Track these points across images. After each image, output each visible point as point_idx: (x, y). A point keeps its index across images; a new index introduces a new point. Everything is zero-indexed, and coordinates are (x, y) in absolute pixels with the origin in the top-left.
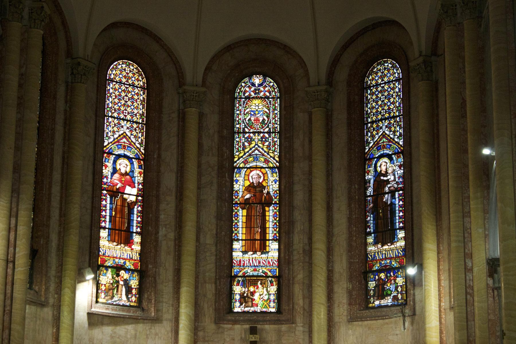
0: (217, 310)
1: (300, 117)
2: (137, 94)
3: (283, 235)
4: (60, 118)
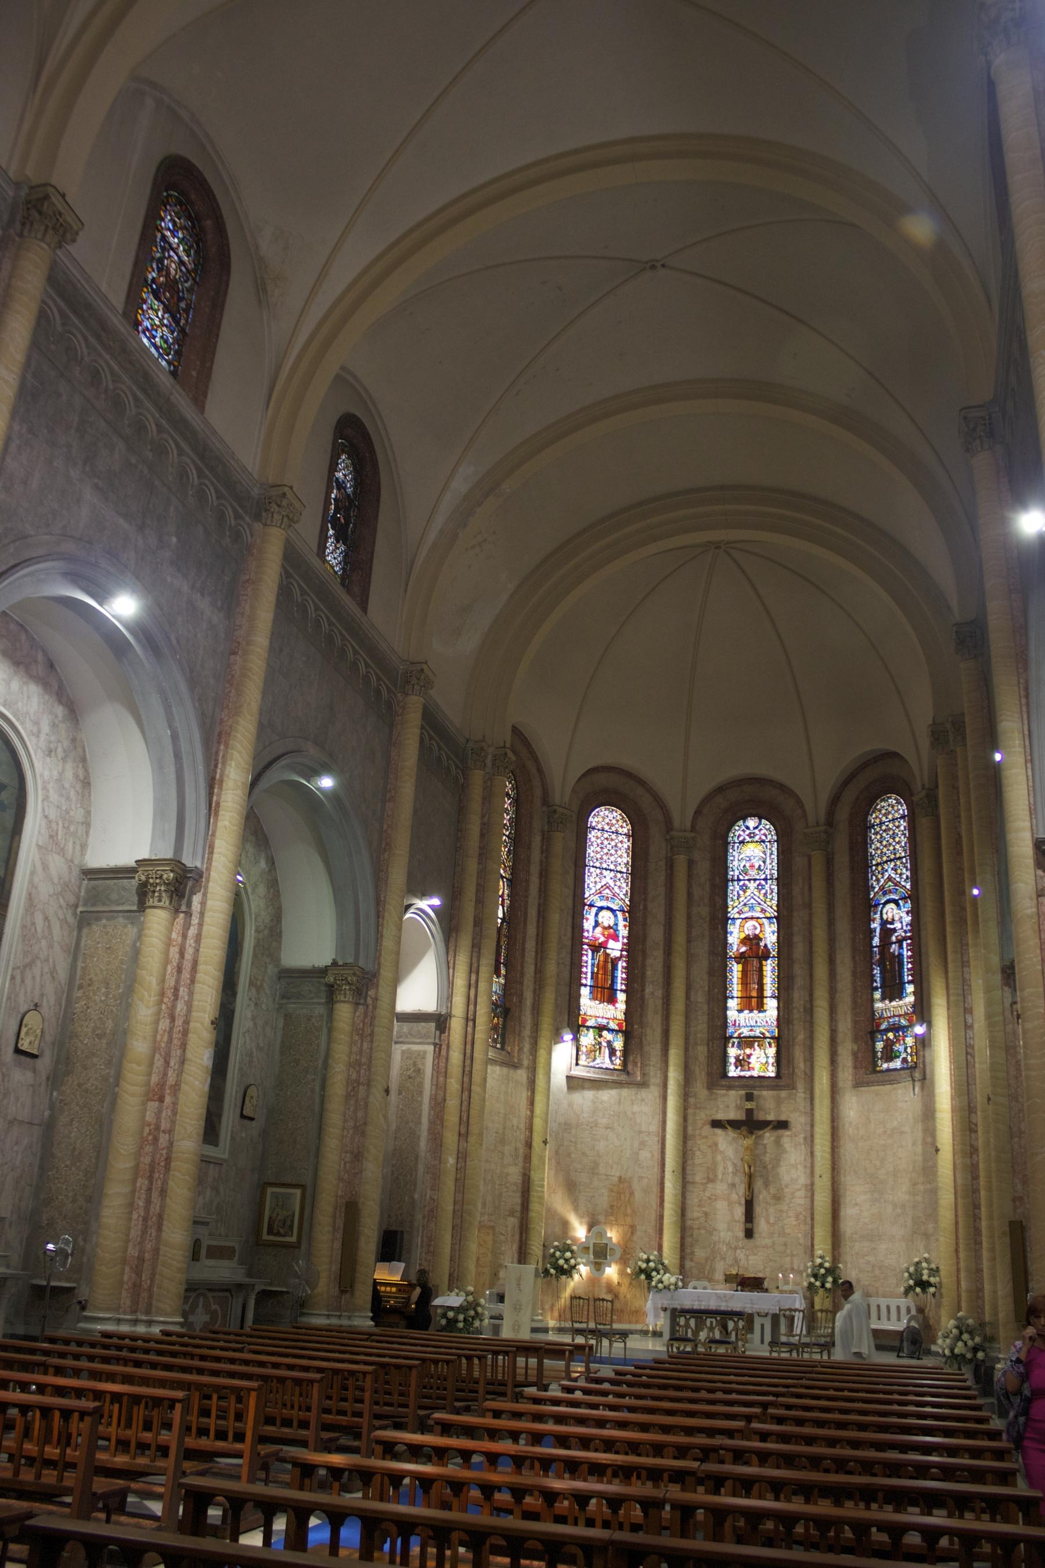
0: (709, 1074)
1: (799, 862)
2: (621, 842)
3: (782, 991)
4: (535, 870)
